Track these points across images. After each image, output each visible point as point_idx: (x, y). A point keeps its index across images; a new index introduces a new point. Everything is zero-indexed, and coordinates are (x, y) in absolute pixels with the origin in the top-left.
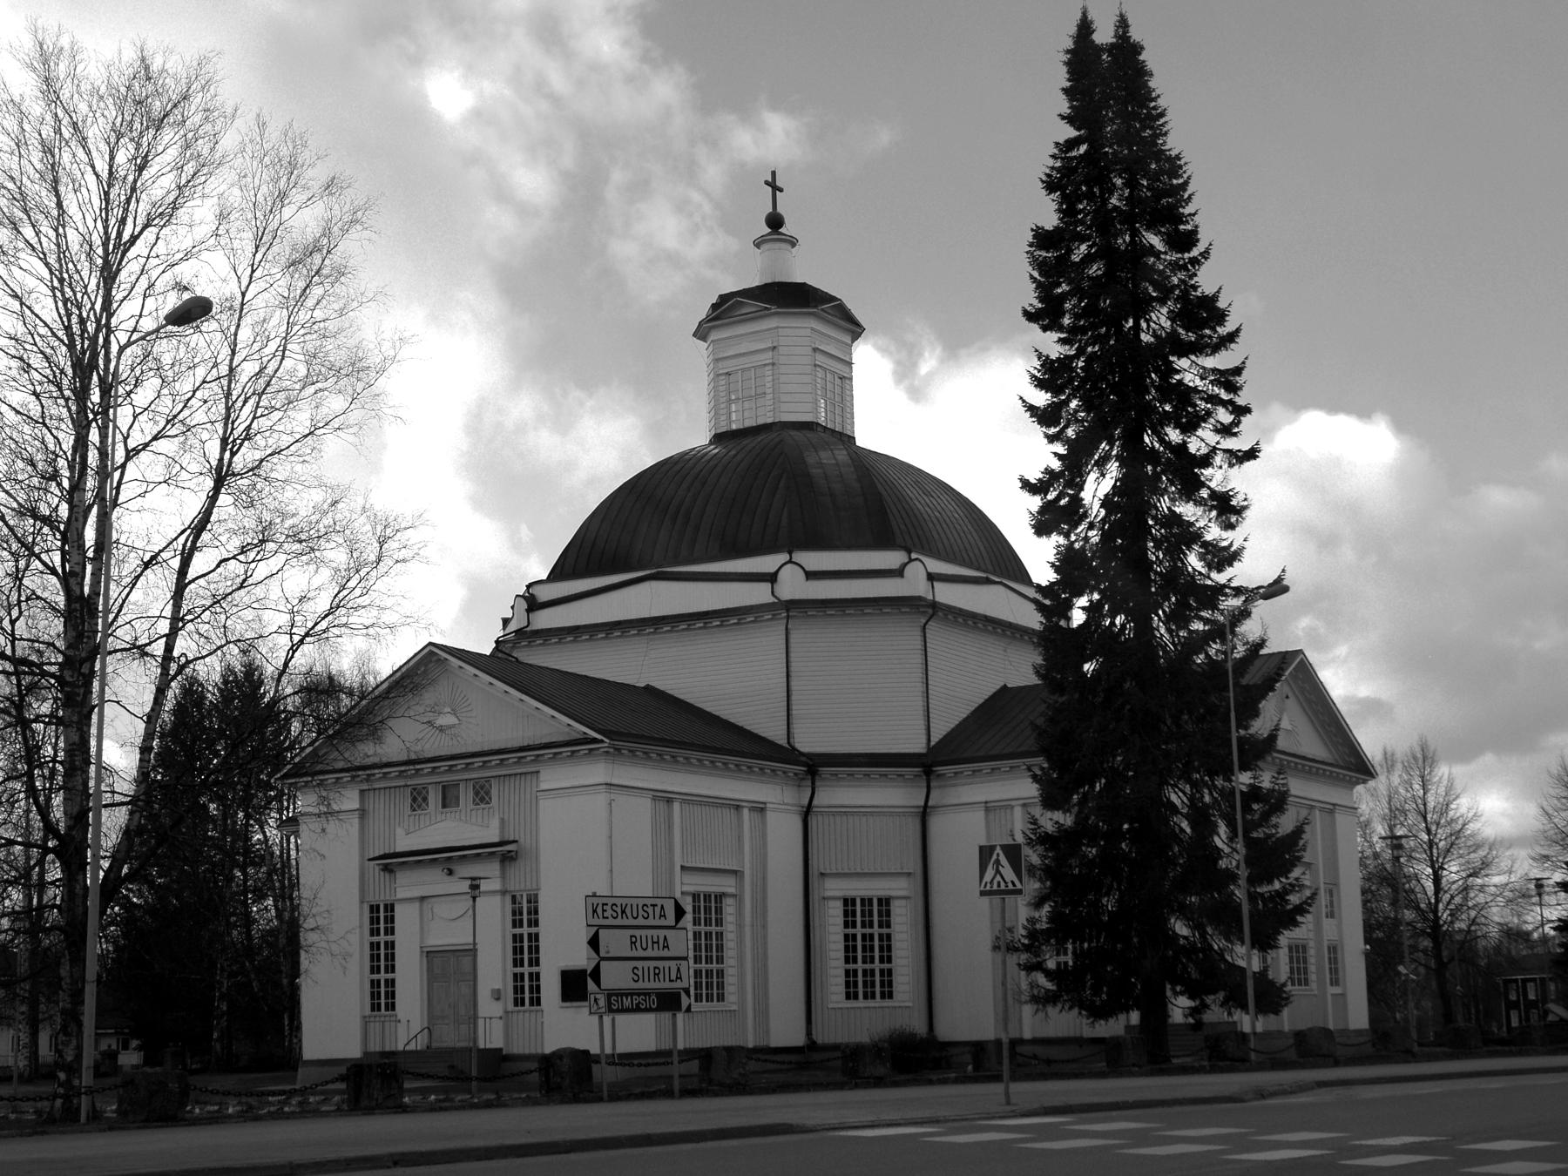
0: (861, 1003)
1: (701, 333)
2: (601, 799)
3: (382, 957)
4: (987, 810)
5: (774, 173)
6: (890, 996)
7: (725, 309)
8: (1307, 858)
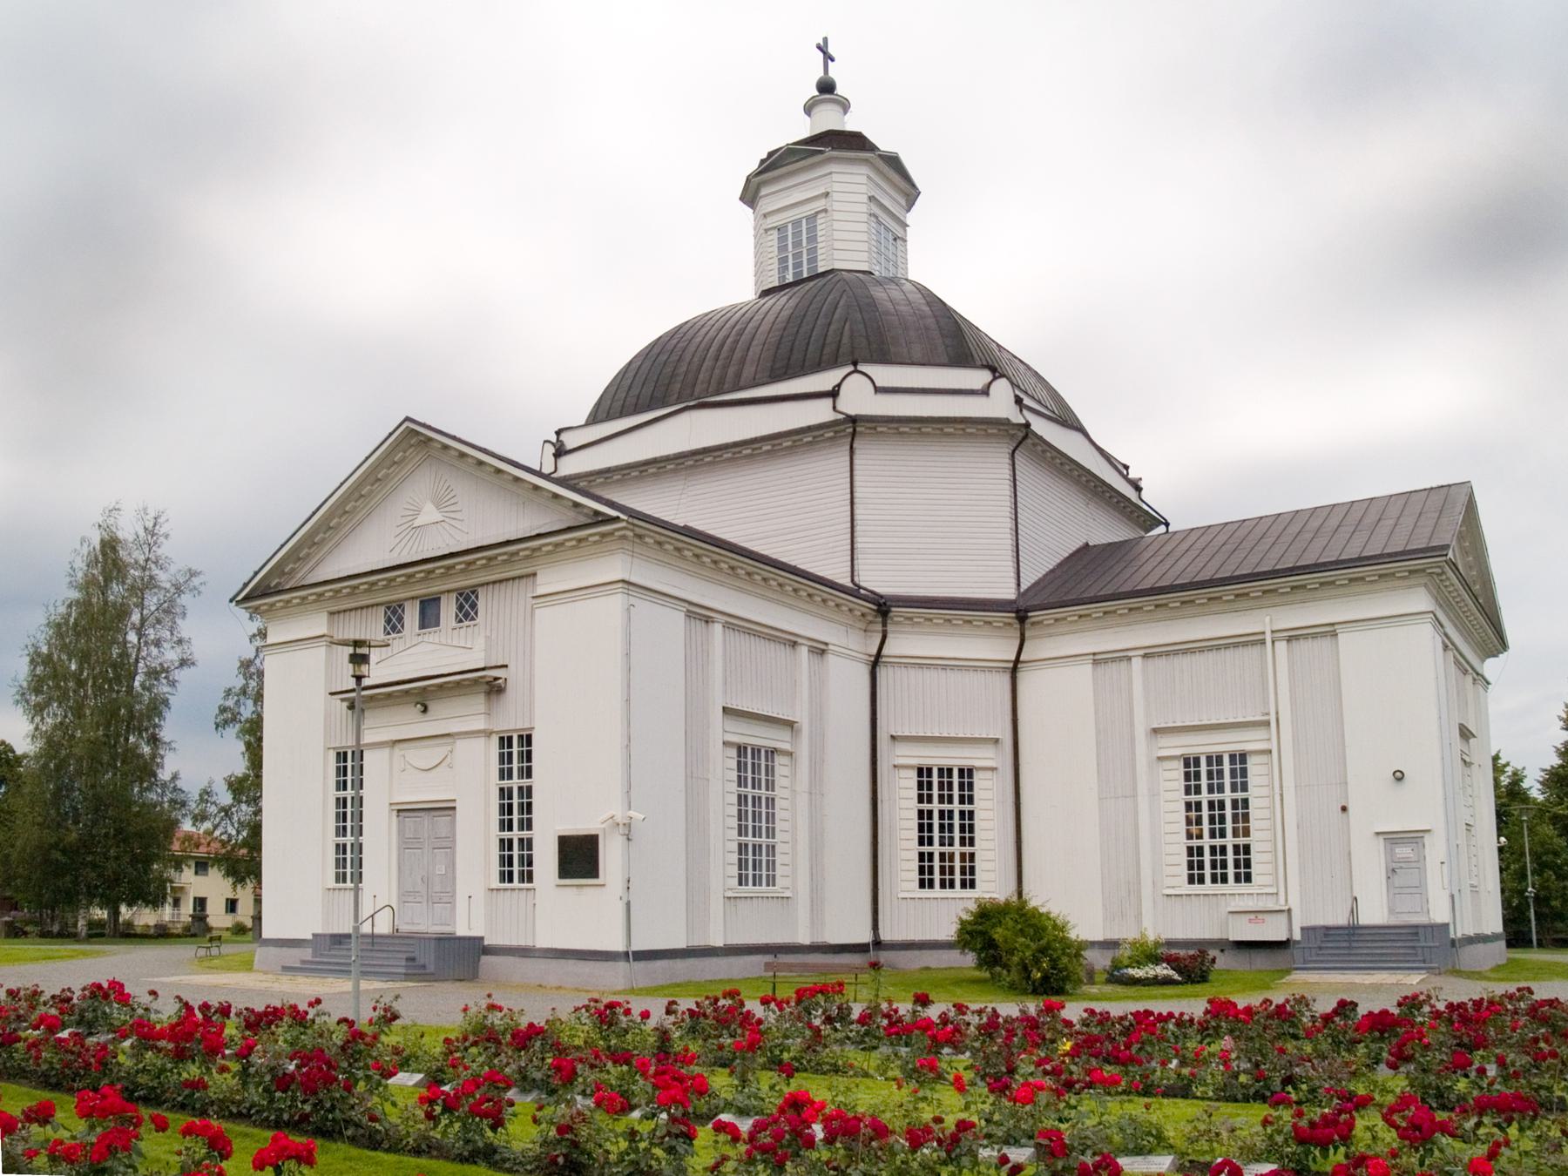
0: (937, 892)
1: (750, 195)
2: (615, 603)
3: (348, 816)
4: (1096, 662)
5: (825, 40)
6: (1248, 878)
7: (777, 164)
8: (364, 1017)
